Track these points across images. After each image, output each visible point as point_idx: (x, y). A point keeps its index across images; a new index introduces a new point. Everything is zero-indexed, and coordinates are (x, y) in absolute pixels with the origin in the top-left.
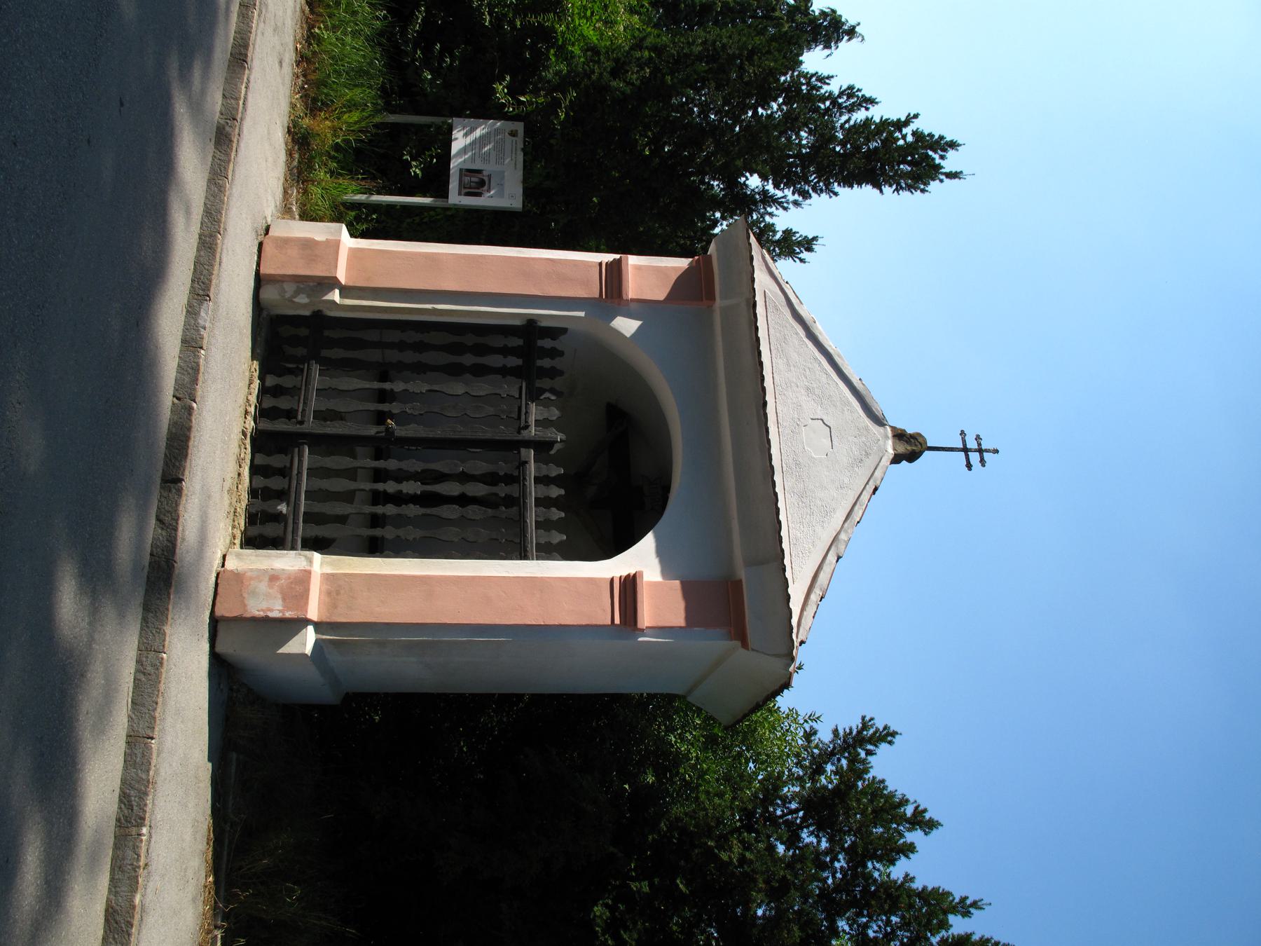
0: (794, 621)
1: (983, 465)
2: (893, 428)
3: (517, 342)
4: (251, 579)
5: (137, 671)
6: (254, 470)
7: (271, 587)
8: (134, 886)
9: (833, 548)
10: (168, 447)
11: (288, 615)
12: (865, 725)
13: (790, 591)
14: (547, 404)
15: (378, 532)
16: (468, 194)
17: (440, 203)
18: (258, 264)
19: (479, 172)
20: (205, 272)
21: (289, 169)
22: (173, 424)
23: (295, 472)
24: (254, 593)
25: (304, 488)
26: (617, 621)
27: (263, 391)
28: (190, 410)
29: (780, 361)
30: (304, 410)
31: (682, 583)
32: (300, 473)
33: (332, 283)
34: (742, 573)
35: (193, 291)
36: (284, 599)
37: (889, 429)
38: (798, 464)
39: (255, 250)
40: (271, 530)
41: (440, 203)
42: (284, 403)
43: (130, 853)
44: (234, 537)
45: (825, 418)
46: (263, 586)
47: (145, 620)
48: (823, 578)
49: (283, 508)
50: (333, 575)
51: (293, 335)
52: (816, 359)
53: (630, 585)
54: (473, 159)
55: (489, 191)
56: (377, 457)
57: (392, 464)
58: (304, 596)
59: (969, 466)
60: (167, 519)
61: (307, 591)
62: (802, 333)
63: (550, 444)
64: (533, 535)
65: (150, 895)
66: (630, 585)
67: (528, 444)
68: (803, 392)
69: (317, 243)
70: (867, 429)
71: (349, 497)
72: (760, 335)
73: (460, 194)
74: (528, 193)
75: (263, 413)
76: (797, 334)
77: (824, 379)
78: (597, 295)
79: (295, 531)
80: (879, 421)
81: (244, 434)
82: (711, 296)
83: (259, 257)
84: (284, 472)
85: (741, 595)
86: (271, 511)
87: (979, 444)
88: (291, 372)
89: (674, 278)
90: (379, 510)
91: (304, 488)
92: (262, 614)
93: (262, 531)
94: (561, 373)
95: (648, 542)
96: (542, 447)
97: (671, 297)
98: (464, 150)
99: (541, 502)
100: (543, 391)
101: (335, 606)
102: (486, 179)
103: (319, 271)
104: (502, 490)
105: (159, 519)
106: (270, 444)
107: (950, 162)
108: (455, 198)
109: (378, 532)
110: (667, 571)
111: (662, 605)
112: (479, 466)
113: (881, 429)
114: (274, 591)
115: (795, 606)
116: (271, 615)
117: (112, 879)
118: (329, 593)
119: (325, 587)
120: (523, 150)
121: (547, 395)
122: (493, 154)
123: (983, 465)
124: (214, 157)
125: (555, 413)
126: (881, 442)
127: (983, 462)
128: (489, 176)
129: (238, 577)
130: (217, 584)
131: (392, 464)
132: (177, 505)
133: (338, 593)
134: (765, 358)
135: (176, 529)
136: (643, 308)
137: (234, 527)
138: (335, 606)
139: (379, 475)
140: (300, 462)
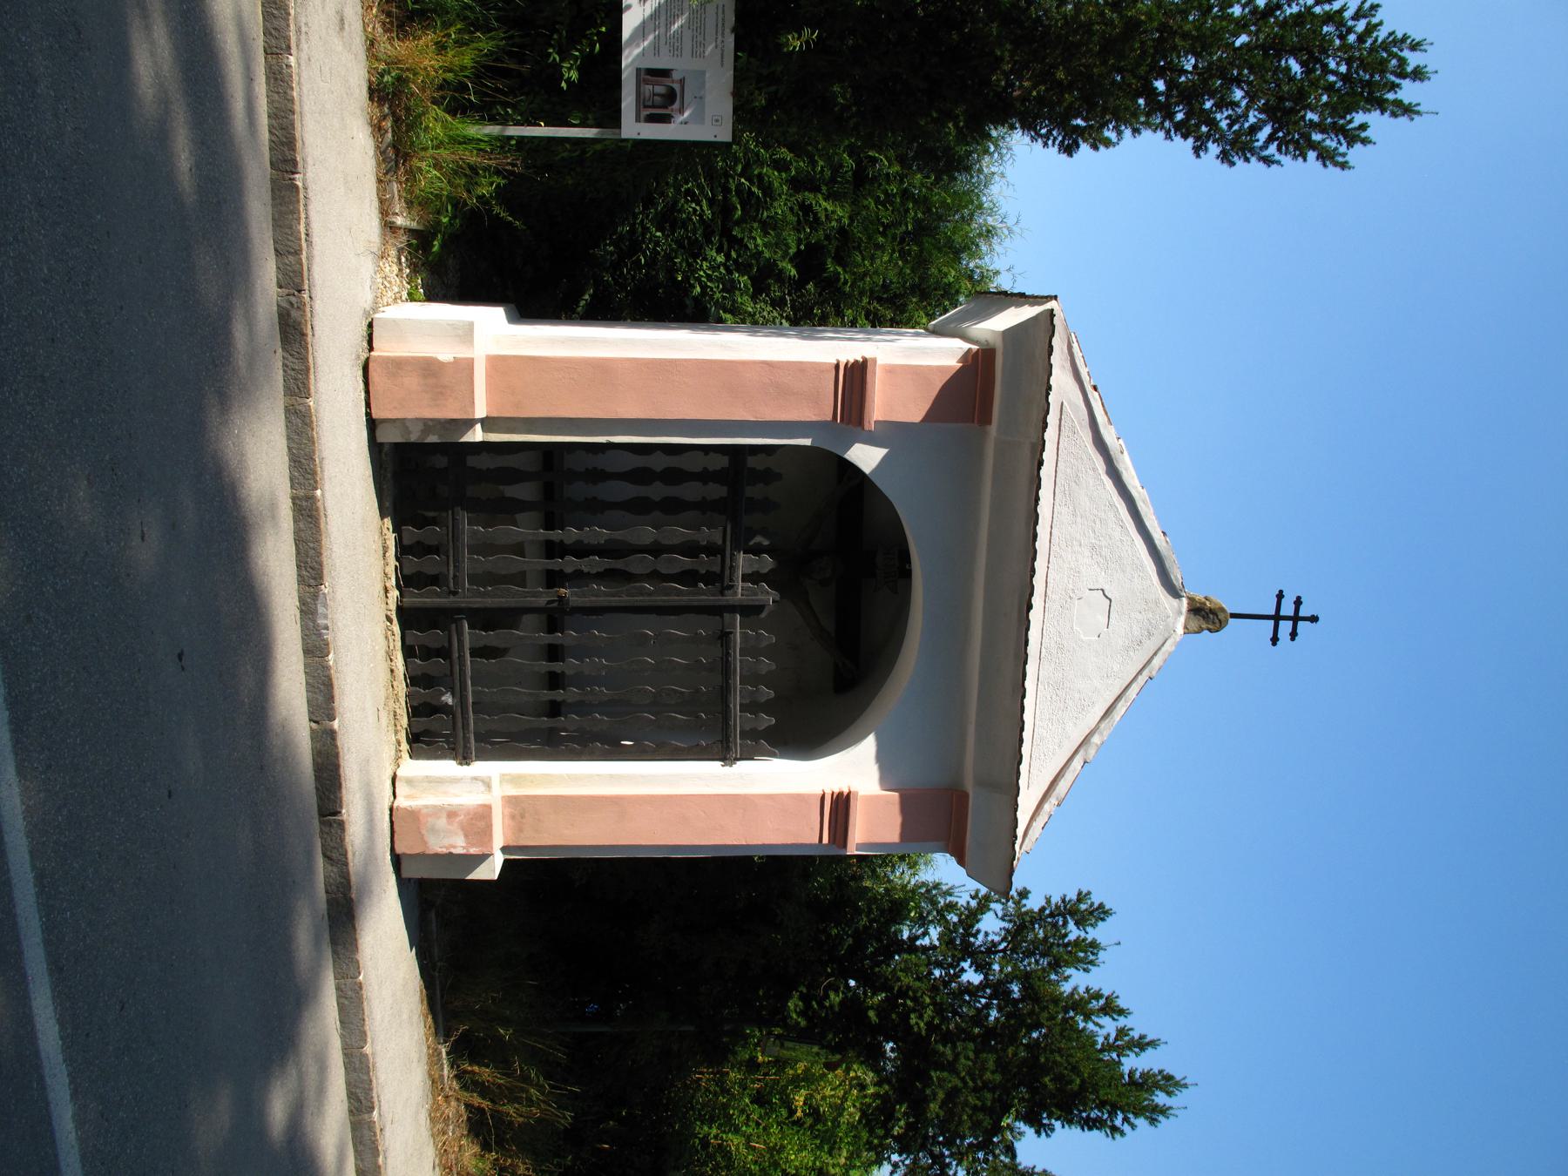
0: (1020, 831)
1: (1293, 639)
2: (1191, 600)
3: (717, 491)
4: (428, 815)
5: (339, 997)
6: (408, 652)
7: (449, 823)
8: (375, 1152)
9: (1082, 752)
10: (318, 778)
11: (473, 851)
12: (1081, 897)
13: (1020, 799)
14: (757, 550)
15: (557, 667)
16: (652, 119)
17: (608, 134)
18: (368, 405)
19: (665, 73)
20: (312, 552)
21: (381, 152)
22: (314, 735)
23: (456, 655)
24: (434, 830)
25: (467, 645)
26: (825, 840)
27: (403, 550)
28: (332, 734)
29: (1064, 510)
30: (455, 576)
31: (901, 796)
32: (461, 657)
33: (469, 424)
34: (969, 787)
35: (301, 580)
36: (466, 836)
37: (1185, 600)
38: (1061, 648)
39: (360, 373)
40: (436, 722)
41: (608, 134)
42: (432, 563)
43: (366, 1132)
44: (399, 743)
45: (1106, 588)
46: (442, 822)
47: (335, 952)
48: (1063, 786)
49: (448, 699)
50: (516, 798)
51: (423, 475)
52: (1112, 505)
53: (840, 806)
54: (656, 48)
55: (681, 111)
56: (549, 526)
57: (571, 534)
58: (487, 832)
59: (1275, 640)
60: (335, 855)
61: (489, 827)
62: (1101, 466)
63: (759, 608)
64: (738, 718)
65: (310, 175)
66: (840, 806)
67: (733, 609)
68: (1087, 553)
69: (442, 365)
70: (1157, 602)
71: (520, 579)
72: (1045, 456)
73: (638, 120)
74: (743, 113)
75: (406, 581)
76: (1094, 469)
77: (1117, 533)
78: (829, 418)
79: (465, 726)
80: (1174, 592)
81: (389, 619)
82: (986, 419)
83: (367, 392)
84: (444, 653)
85: (962, 799)
86: (434, 702)
87: (1297, 610)
88: (434, 522)
89: (938, 385)
90: (557, 564)
91: (467, 645)
92: (445, 851)
93: (430, 731)
94: (779, 476)
95: (868, 747)
96: (750, 611)
97: (934, 414)
98: (641, 31)
99: (751, 678)
100: (752, 533)
101: (521, 830)
102: (677, 87)
103: (450, 412)
104: (705, 563)
105: (325, 855)
106: (422, 625)
107: (1408, 92)
108: (633, 128)
109: (557, 667)
110: (886, 781)
111: (877, 825)
112: (679, 533)
113: (1175, 602)
114: (455, 827)
115: (1023, 817)
116: (455, 851)
117: (356, 1151)
118: (513, 817)
119: (508, 811)
120: (734, 30)
121: (758, 539)
122: (688, 34)
123: (1293, 639)
124: (285, 365)
125: (768, 562)
126: (1170, 620)
127: (1293, 635)
128: (682, 82)
129: (413, 815)
130: (392, 822)
131: (571, 534)
132: (342, 840)
133: (522, 816)
134: (1044, 509)
135: (346, 864)
136: (890, 434)
137: (396, 732)
138: (521, 830)
139: (552, 549)
140: (461, 642)
